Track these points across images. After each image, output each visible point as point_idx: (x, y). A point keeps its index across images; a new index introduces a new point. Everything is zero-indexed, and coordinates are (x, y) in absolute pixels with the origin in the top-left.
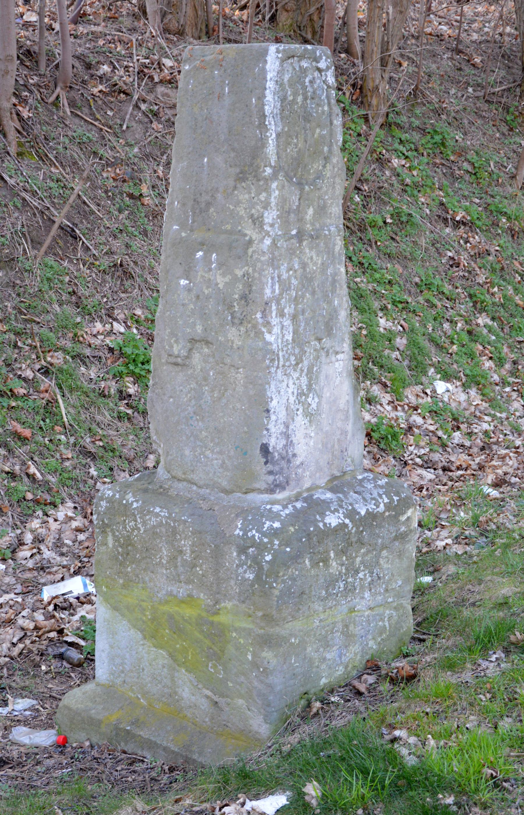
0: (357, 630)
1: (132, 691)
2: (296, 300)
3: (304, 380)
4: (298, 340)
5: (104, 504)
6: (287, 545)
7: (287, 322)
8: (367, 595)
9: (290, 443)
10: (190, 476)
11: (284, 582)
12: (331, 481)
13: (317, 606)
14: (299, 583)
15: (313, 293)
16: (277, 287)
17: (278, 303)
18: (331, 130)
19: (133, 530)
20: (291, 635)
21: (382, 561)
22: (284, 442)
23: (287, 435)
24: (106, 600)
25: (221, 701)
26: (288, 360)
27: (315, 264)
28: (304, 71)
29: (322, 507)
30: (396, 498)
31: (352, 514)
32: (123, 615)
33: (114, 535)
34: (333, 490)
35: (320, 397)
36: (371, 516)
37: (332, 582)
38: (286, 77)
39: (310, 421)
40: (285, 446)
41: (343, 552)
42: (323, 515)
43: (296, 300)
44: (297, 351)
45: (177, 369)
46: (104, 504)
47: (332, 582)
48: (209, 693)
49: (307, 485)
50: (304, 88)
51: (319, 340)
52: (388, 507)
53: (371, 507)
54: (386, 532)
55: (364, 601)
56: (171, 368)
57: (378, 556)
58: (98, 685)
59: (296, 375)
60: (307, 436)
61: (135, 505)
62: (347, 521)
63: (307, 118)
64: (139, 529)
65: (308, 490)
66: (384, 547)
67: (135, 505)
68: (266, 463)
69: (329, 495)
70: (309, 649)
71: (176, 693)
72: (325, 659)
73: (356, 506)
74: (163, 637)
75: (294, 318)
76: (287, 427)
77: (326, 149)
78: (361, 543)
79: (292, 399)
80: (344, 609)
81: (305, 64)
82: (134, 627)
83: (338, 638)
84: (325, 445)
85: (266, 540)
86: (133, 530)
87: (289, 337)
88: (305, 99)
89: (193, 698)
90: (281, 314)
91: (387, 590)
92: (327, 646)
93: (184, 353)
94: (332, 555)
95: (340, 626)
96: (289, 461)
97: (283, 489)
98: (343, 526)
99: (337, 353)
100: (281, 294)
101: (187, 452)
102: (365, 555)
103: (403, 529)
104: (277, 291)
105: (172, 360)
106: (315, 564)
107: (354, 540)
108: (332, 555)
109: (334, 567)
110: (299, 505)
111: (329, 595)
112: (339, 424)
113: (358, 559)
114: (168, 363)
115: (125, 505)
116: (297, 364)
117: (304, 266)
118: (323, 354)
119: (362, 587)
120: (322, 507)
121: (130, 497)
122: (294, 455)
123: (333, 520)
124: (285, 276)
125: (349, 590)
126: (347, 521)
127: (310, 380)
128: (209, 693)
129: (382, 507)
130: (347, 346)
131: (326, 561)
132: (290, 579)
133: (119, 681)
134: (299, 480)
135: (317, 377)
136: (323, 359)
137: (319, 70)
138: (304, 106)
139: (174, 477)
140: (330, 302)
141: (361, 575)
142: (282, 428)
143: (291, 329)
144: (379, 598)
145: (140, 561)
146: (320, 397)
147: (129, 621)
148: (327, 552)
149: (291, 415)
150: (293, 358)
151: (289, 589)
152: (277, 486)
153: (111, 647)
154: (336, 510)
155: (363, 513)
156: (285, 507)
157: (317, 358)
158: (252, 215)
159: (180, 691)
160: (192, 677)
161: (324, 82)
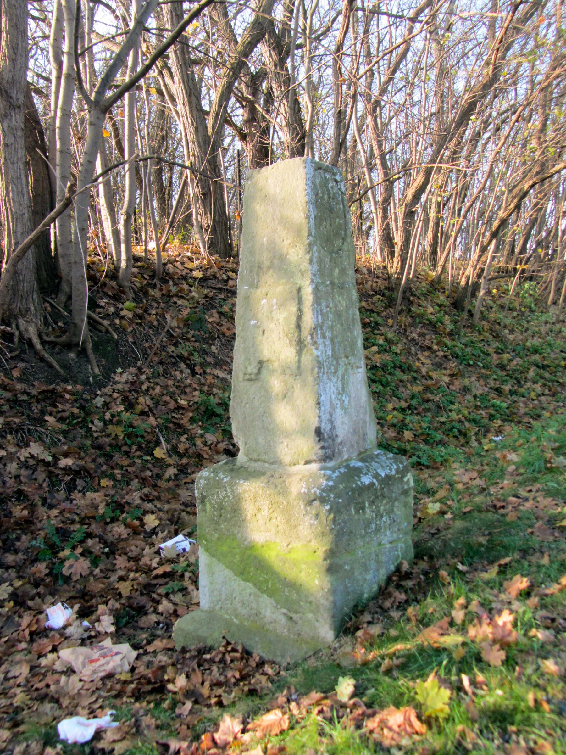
0: (383, 558)
1: (227, 613)
2: (331, 328)
3: (340, 384)
4: (335, 357)
5: (202, 481)
6: (339, 498)
7: (328, 342)
8: (388, 533)
9: (333, 428)
10: (264, 457)
11: (339, 524)
12: (360, 453)
13: (360, 542)
14: (348, 525)
15: (342, 325)
16: (320, 317)
17: (321, 329)
18: (345, 221)
19: (224, 498)
20: (345, 563)
21: (395, 509)
22: (330, 426)
23: (331, 422)
24: (206, 550)
25: (295, 616)
26: (330, 368)
27: (342, 305)
28: (327, 180)
29: (357, 471)
30: (401, 466)
31: (376, 476)
32: (219, 560)
33: (210, 503)
34: (362, 460)
35: (350, 397)
36: (388, 477)
37: (368, 524)
38: (318, 181)
39: (345, 413)
40: (331, 429)
41: (373, 502)
42: (359, 477)
43: (331, 328)
44: (335, 362)
45: (250, 383)
46: (202, 481)
47: (368, 524)
48: (285, 611)
49: (346, 457)
50: (328, 190)
51: (347, 357)
52: (397, 471)
53: (388, 471)
54: (396, 489)
55: (386, 537)
56: (246, 383)
57: (393, 506)
58: (202, 611)
59: (334, 380)
60: (343, 423)
61: (225, 480)
62: (375, 481)
63: (331, 211)
64: (228, 497)
65: (347, 460)
66: (397, 499)
67: (225, 480)
68: (319, 441)
69: (360, 464)
70: (356, 573)
71: (260, 613)
72: (365, 580)
73: (379, 471)
74: (249, 573)
75: (332, 340)
76: (331, 416)
77: (343, 233)
78: (384, 497)
79: (333, 396)
80: (375, 543)
81: (328, 176)
82: (227, 567)
83: (373, 564)
84: (354, 430)
85: (324, 494)
86: (224, 498)
87: (330, 353)
88: (329, 198)
89: (274, 616)
90: (324, 337)
91: (399, 530)
92: (367, 570)
93: (255, 371)
94: (367, 504)
95: (373, 556)
96: (333, 440)
97: (331, 459)
98: (372, 484)
99: (358, 367)
100: (323, 323)
101: (260, 440)
102: (386, 504)
103: (406, 487)
104: (320, 321)
105: (247, 377)
106: (357, 512)
107: (379, 493)
108: (367, 504)
109: (369, 513)
110: (342, 470)
111: (367, 533)
112: (361, 416)
113: (382, 508)
114: (244, 380)
115: (218, 481)
116: (335, 372)
117: (336, 306)
118: (350, 367)
119: (385, 528)
120: (357, 471)
121: (221, 475)
122: (337, 436)
123: (366, 480)
124: (324, 311)
125: (378, 530)
126: (375, 481)
127: (343, 384)
128: (285, 611)
129: (393, 472)
130: (362, 363)
131: (363, 508)
132: (343, 521)
133: (218, 607)
134: (340, 453)
135: (347, 383)
136: (350, 370)
137: (336, 181)
138: (328, 202)
139: (251, 459)
140: (352, 333)
141: (384, 519)
142: (328, 416)
143: (330, 347)
144: (395, 535)
145: (231, 519)
146: (350, 397)
147: (224, 564)
148: (364, 502)
149: (333, 407)
150: (332, 368)
151: (342, 529)
152: (327, 457)
153: (211, 583)
154: (366, 474)
155: (383, 475)
156: (334, 471)
157: (346, 370)
158: (301, 270)
159: (263, 611)
160: (272, 601)
161: (340, 189)
